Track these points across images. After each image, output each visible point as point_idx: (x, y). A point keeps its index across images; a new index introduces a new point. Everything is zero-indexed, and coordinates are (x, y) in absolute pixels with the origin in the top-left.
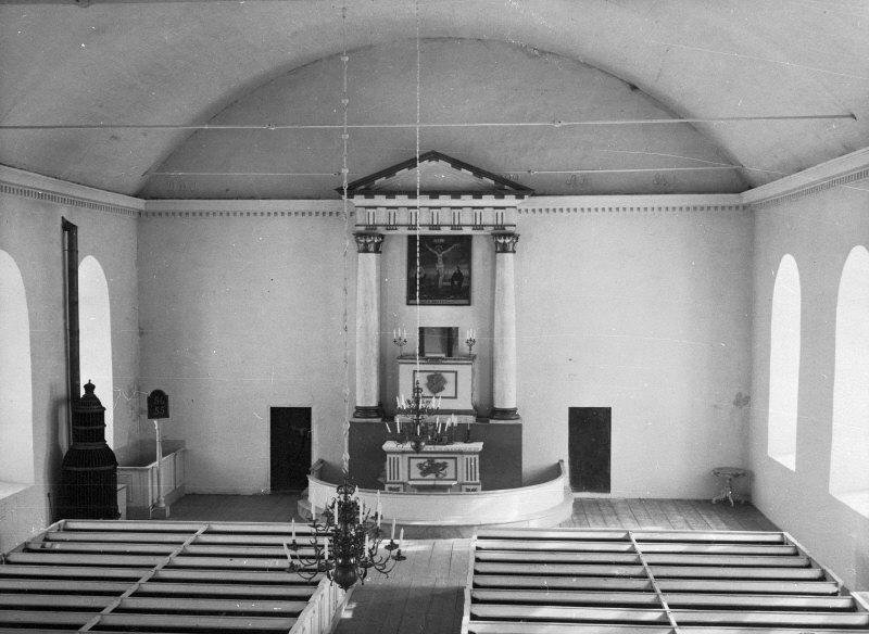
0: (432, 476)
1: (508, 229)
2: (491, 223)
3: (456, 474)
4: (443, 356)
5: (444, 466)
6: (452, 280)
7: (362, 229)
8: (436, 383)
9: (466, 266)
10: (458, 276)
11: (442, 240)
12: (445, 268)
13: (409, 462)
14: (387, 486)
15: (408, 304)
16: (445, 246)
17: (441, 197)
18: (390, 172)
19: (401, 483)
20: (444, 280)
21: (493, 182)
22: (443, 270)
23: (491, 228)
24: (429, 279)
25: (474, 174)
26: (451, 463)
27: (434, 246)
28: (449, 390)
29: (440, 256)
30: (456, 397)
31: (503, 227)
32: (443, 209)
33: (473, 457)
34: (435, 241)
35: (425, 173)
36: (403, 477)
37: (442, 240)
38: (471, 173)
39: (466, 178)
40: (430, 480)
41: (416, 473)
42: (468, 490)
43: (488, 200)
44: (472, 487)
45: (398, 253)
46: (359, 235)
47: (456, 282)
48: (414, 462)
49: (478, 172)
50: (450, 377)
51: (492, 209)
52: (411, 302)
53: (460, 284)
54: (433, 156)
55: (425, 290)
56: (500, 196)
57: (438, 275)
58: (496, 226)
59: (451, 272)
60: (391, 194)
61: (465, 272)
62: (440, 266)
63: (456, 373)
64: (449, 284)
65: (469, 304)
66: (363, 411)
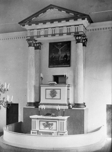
0: (48, 128)
1: (80, 33)
2: (74, 32)
3: (56, 128)
4: (56, 83)
5: (52, 124)
6: (64, 58)
7: (29, 38)
8: (53, 94)
9: (69, 52)
10: (66, 56)
11: (61, 44)
12: (61, 53)
13: (40, 123)
14: (31, 131)
15: (49, 67)
16: (62, 46)
17: (54, 22)
18: (36, 15)
19: (36, 131)
20: (61, 58)
21: (73, 14)
22: (61, 54)
23: (74, 33)
24: (56, 58)
25: (67, 12)
26: (54, 123)
27: (57, 46)
28: (58, 96)
29: (60, 49)
30: (46, 99)
31: (78, 32)
32: (56, 28)
33: (33, 129)
34: (58, 44)
35: (52, 13)
36: (37, 129)
37: (61, 44)
38: (65, 12)
39: (63, 14)
40: (47, 130)
41: (42, 127)
42: (60, 135)
43: (72, 22)
44: (62, 133)
45: (46, 49)
46: (28, 40)
47: (65, 59)
48: (42, 123)
49: (68, 11)
50: (58, 91)
51: (74, 26)
52: (50, 66)
53: (66, 59)
54: (51, 7)
55: (53, 62)
56: (75, 19)
57: (59, 56)
58: (75, 33)
59: (64, 55)
60: (37, 23)
61: (68, 55)
62: (60, 53)
63: (60, 89)
64: (63, 59)
65: (70, 66)
66: (30, 104)
